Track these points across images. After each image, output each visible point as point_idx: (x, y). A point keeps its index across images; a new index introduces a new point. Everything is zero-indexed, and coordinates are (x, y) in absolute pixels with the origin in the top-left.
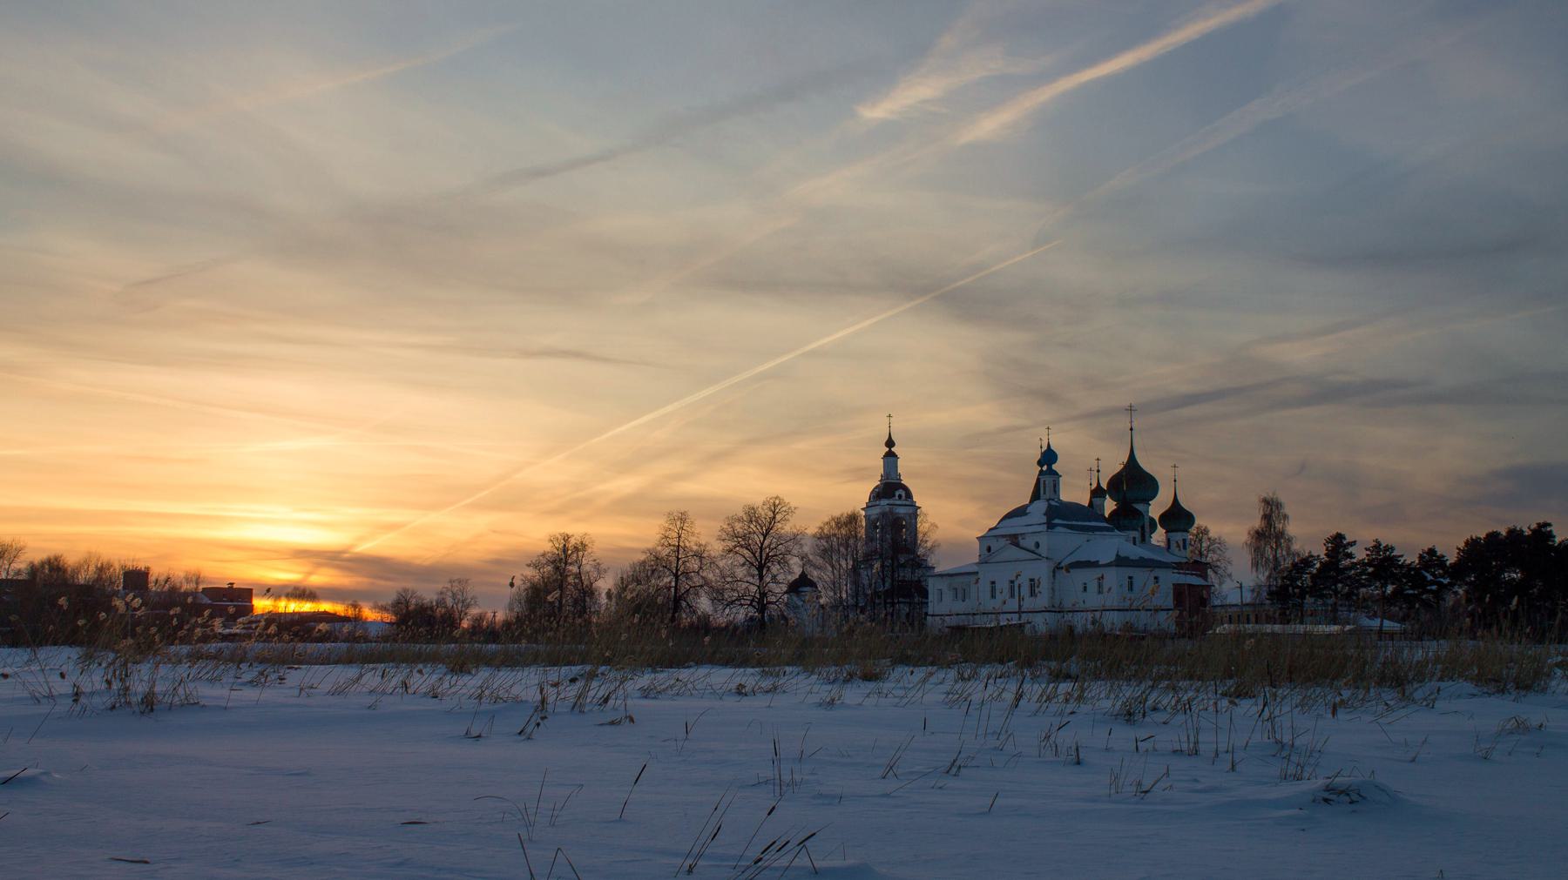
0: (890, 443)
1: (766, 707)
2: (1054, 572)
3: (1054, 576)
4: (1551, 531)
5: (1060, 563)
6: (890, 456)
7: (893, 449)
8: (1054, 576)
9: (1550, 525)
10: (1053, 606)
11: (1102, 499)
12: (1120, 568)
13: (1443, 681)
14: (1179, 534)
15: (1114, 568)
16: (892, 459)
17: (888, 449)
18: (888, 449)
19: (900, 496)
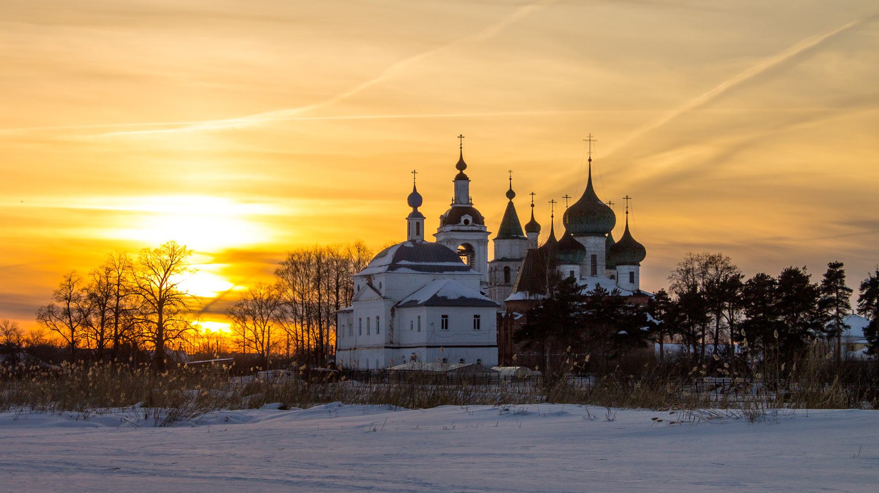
0: (461, 165)
1: (495, 426)
2: (393, 310)
3: (393, 315)
4: (754, 279)
5: (399, 302)
6: (462, 180)
7: (463, 171)
8: (393, 315)
9: (842, 265)
10: (391, 342)
11: (537, 234)
12: (429, 307)
13: (799, 408)
14: (626, 267)
15: (425, 308)
16: (462, 182)
17: (459, 172)
18: (459, 172)
19: (466, 222)
